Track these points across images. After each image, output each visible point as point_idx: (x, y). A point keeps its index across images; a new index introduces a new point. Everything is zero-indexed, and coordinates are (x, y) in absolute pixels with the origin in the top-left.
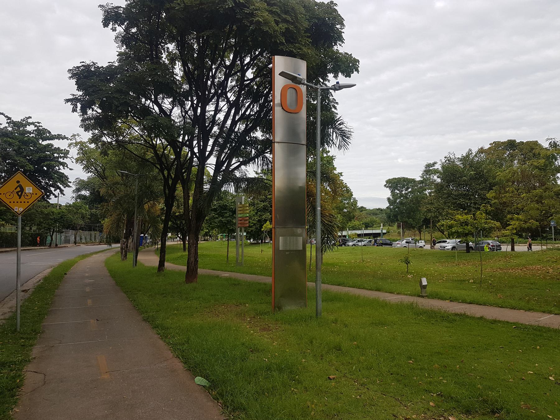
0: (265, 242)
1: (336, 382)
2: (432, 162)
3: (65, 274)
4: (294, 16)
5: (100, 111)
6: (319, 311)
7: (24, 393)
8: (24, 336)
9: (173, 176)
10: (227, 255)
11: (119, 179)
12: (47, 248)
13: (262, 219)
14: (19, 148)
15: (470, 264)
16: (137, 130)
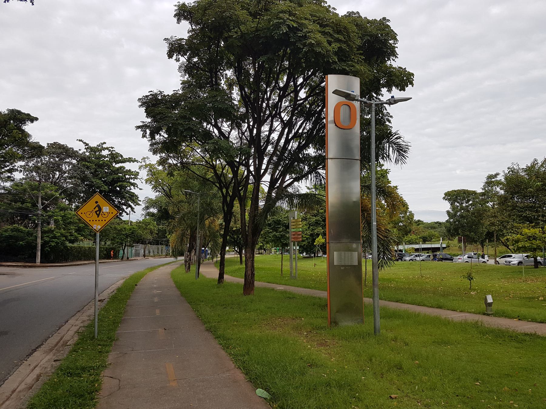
0: (317, 256)
1: (398, 402)
2: (494, 173)
3: (136, 285)
4: (347, 35)
5: (166, 136)
6: (377, 327)
7: (101, 397)
8: (101, 343)
9: (231, 194)
10: (282, 269)
11: (183, 198)
12: (120, 261)
13: (315, 233)
14: (96, 171)
15: (539, 280)
16: (199, 152)
